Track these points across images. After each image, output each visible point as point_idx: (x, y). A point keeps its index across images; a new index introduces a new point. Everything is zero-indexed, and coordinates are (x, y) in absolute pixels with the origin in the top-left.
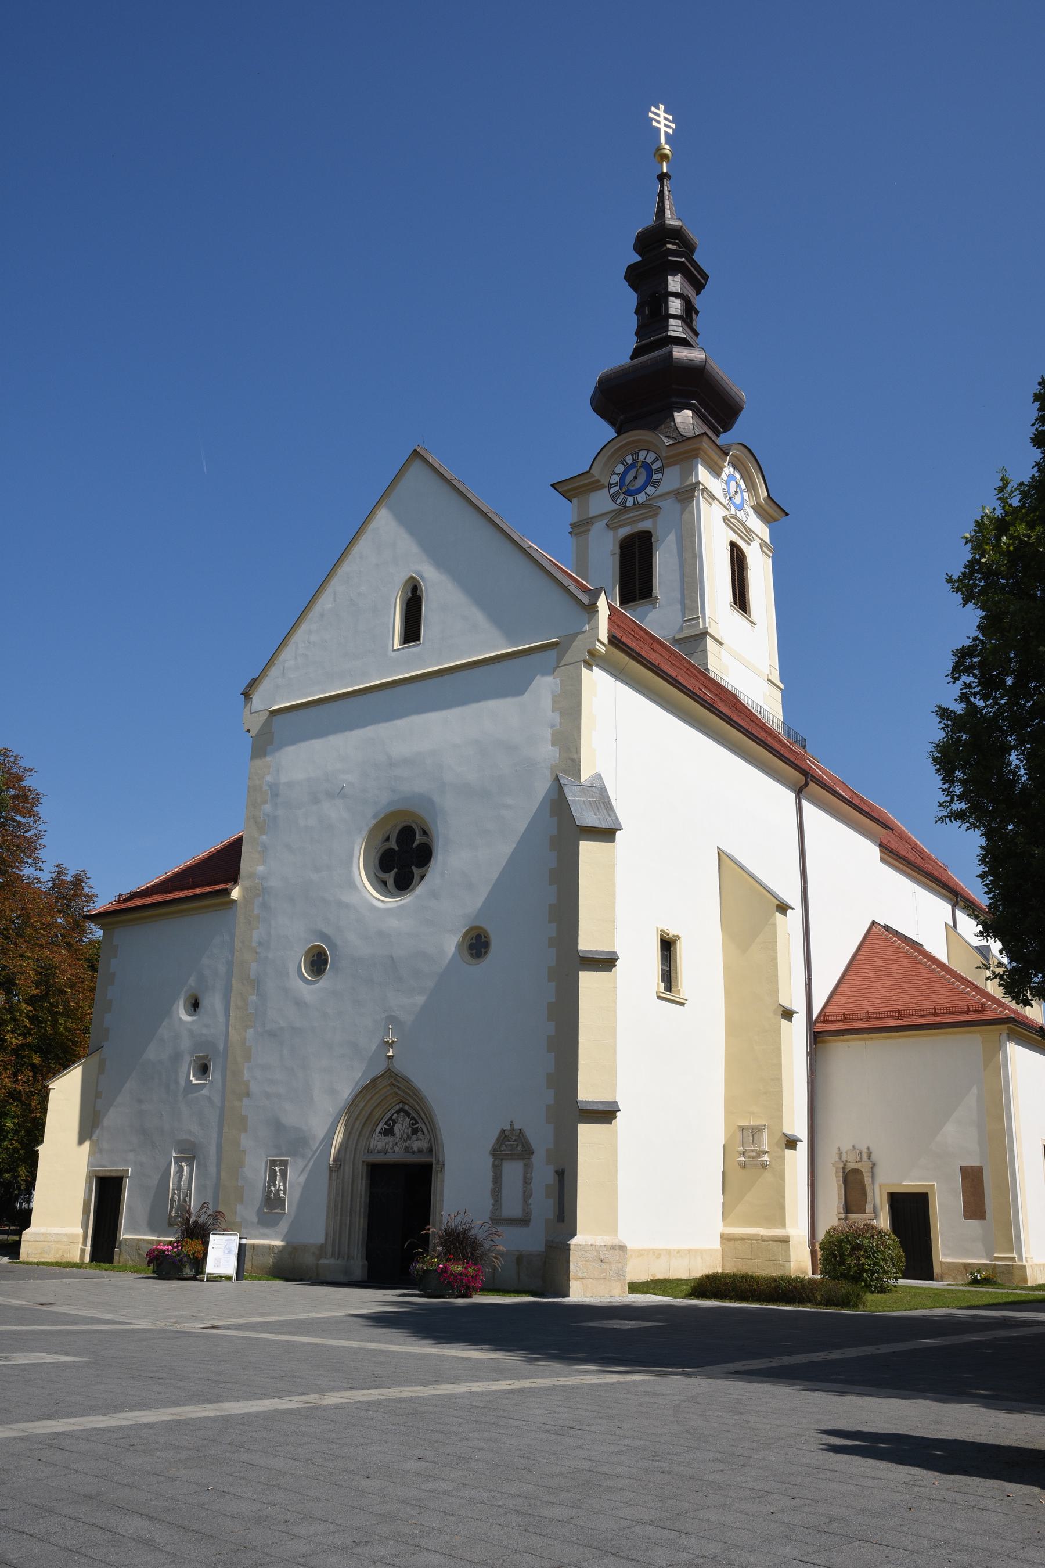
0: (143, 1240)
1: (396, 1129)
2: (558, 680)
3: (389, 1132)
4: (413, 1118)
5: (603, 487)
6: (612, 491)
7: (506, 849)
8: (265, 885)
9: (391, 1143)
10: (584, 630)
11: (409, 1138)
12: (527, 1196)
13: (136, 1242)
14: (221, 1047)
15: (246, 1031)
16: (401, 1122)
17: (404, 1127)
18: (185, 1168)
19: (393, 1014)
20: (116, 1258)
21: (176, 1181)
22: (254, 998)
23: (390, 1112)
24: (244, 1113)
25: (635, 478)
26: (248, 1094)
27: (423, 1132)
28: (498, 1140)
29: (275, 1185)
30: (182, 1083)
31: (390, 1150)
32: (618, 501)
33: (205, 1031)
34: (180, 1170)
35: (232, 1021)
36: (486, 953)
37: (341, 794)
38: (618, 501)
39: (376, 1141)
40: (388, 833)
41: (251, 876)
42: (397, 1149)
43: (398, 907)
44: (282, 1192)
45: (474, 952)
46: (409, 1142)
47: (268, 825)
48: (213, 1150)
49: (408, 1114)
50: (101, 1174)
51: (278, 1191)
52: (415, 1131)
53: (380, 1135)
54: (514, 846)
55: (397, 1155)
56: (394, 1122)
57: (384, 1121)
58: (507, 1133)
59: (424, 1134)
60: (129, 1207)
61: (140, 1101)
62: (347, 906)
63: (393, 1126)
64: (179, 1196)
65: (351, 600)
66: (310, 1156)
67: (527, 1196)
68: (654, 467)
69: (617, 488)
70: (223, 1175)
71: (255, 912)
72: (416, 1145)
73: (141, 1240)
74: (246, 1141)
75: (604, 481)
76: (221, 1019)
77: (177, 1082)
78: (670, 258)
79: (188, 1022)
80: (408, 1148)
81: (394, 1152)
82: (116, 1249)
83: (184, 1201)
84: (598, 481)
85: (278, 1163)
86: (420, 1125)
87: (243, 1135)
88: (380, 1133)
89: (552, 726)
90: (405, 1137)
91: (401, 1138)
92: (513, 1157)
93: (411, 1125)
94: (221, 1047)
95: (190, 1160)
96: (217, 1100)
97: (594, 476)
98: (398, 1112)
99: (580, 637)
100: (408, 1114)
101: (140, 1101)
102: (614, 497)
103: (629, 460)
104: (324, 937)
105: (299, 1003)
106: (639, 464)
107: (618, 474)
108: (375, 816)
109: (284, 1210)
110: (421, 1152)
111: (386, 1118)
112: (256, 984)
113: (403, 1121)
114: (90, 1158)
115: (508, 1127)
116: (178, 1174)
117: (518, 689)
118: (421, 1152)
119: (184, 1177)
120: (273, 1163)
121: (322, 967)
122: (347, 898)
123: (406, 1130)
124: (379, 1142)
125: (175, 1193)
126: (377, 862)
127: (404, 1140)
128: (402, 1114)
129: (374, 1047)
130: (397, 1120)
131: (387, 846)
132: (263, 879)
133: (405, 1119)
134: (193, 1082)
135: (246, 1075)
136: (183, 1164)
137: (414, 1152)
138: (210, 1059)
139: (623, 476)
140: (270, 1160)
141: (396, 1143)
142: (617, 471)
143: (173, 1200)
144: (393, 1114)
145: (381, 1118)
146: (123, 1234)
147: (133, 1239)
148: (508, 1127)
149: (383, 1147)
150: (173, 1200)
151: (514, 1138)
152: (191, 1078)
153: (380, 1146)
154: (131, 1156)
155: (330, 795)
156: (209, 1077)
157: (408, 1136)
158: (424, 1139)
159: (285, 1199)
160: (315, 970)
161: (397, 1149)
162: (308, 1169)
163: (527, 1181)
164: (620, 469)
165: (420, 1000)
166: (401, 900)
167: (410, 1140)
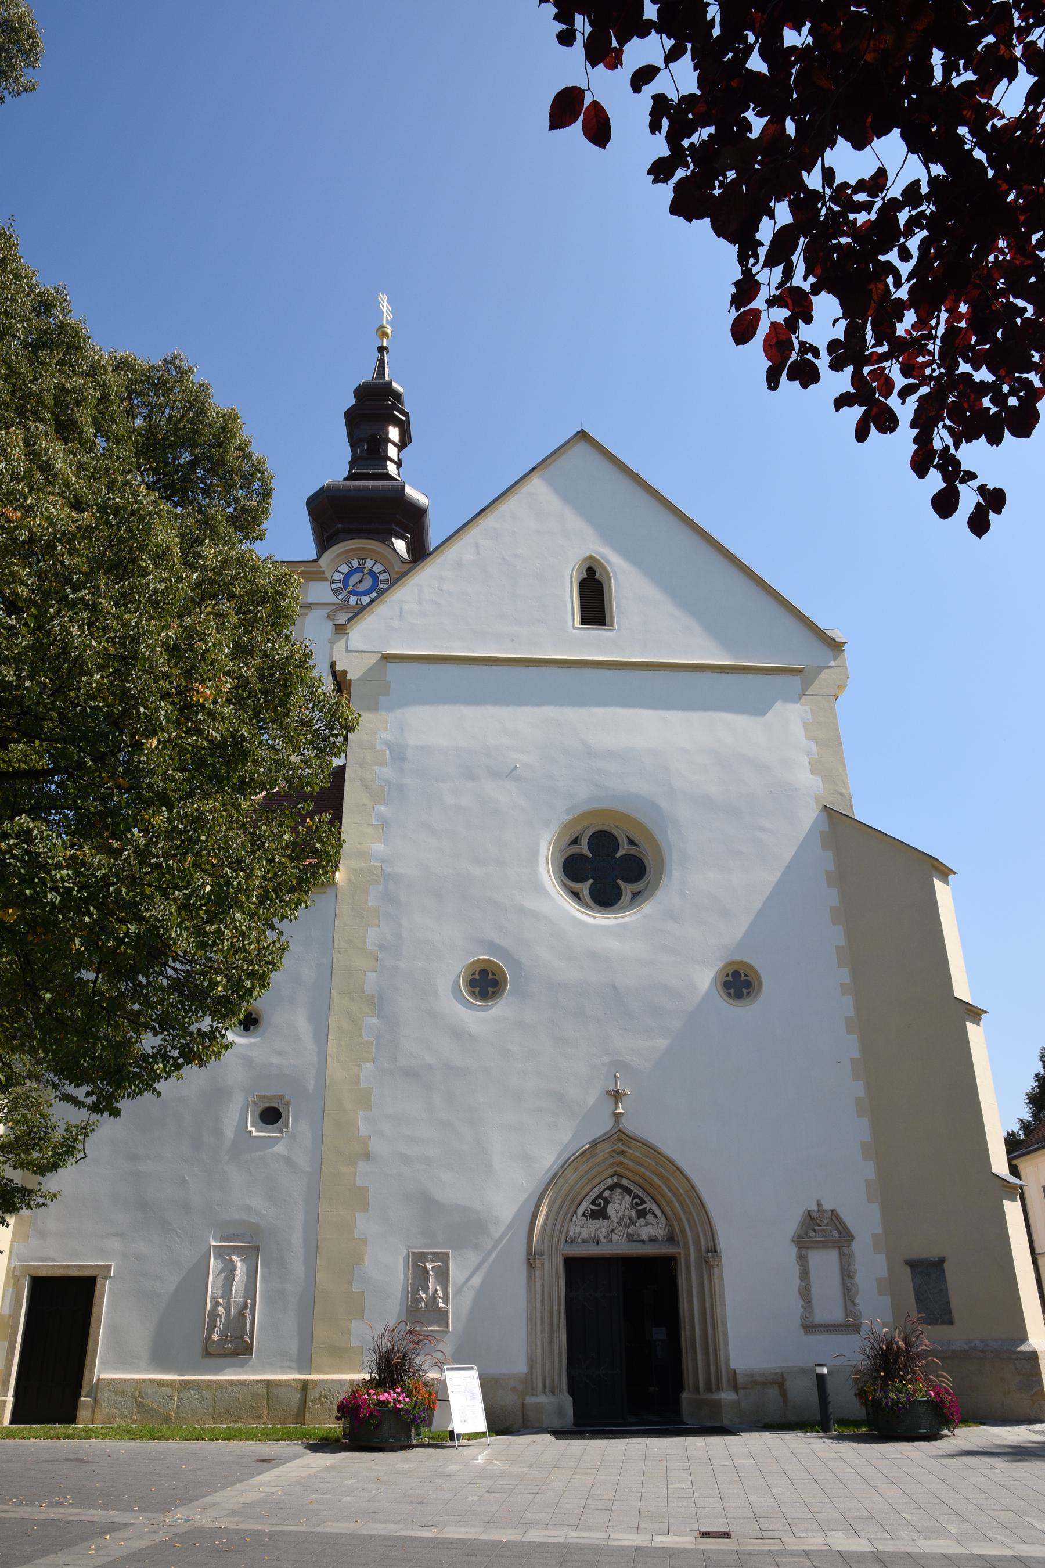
0: (150, 1380)
1: (611, 1210)
2: (808, 708)
3: (599, 1213)
4: (637, 1196)
5: (325, 579)
6: (334, 586)
7: (769, 877)
8: (388, 869)
9: (603, 1230)
10: (830, 665)
11: (632, 1222)
12: (848, 1293)
13: (134, 1385)
14: (311, 1085)
15: (359, 1066)
16: (618, 1202)
17: (623, 1207)
18: (239, 1264)
19: (620, 1058)
20: (83, 1413)
21: (220, 1284)
22: (374, 1020)
23: (598, 1187)
24: (359, 1183)
25: (361, 581)
26: (367, 1156)
27: (654, 1213)
28: (802, 1225)
29: (426, 1289)
30: (229, 1133)
31: (602, 1239)
32: (340, 597)
33: (276, 1060)
34: (230, 1269)
35: (332, 1049)
36: (729, 995)
37: (512, 774)
38: (340, 597)
39: (578, 1227)
40: (577, 835)
41: (362, 855)
42: (614, 1237)
43: (617, 925)
44: (441, 1300)
45: (745, 991)
46: (633, 1227)
47: (388, 794)
48: (297, 1238)
49: (628, 1191)
50: (43, 1273)
51: (434, 1298)
52: (642, 1214)
53: (584, 1218)
54: (779, 874)
55: (617, 1245)
56: (607, 1202)
57: (589, 1199)
58: (814, 1215)
59: (656, 1217)
60: (112, 1328)
61: (134, 1158)
62: (535, 915)
63: (606, 1206)
64: (227, 1309)
65: (504, 558)
66: (489, 1247)
67: (848, 1293)
68: (381, 577)
69: (340, 585)
70: (321, 1276)
71: (371, 904)
72: (645, 1232)
73: (144, 1381)
74: (364, 1224)
75: (328, 575)
76: (309, 1045)
77: (218, 1133)
78: (395, 412)
79: (241, 1045)
80: (632, 1235)
81: (610, 1241)
82: (82, 1399)
83: (241, 1315)
84: (323, 572)
85: (430, 1257)
86: (650, 1205)
87: (359, 1216)
88: (583, 1215)
89: (808, 754)
90: (626, 1221)
91: (620, 1223)
92: (823, 1245)
93: (633, 1206)
94: (311, 1085)
95: (251, 1252)
96: (303, 1160)
97: (320, 567)
98: (611, 1188)
99: (826, 671)
100: (628, 1191)
101: (134, 1158)
102: (336, 592)
103: (355, 564)
104: (493, 947)
105: (458, 1034)
106: (366, 571)
107: (342, 573)
108: (568, 811)
109: (447, 1327)
110: (654, 1241)
111: (593, 1195)
112: (376, 1002)
113: (621, 1200)
114: (16, 1245)
115: (814, 1207)
116: (223, 1275)
117: (759, 708)
118: (654, 1241)
119: (237, 1279)
120: (421, 1257)
121: (490, 989)
122: (531, 903)
123: (627, 1212)
124: (584, 1229)
125: (218, 1304)
126: (561, 866)
127: (626, 1225)
128: (618, 1190)
129: (591, 1100)
130: (612, 1198)
131: (575, 849)
132: (383, 861)
133: (623, 1197)
134: (254, 1133)
135: (363, 1129)
136: (234, 1258)
137: (643, 1241)
138: (289, 1102)
139: (347, 577)
140: (413, 1253)
141: (613, 1230)
142: (341, 569)
143: (214, 1315)
144: (603, 1191)
145: (583, 1193)
146: (100, 1372)
147: (125, 1380)
148: (814, 1207)
149: (591, 1235)
150: (214, 1315)
151: (826, 1221)
152: (249, 1128)
153: (585, 1234)
154: (115, 1244)
155: (495, 774)
156: (287, 1128)
157: (631, 1220)
158: (658, 1223)
159: (447, 1311)
160: (477, 992)
161: (614, 1237)
162: (486, 1265)
163: (847, 1274)
164: (345, 569)
165: (662, 1043)
166: (620, 917)
167: (635, 1225)
